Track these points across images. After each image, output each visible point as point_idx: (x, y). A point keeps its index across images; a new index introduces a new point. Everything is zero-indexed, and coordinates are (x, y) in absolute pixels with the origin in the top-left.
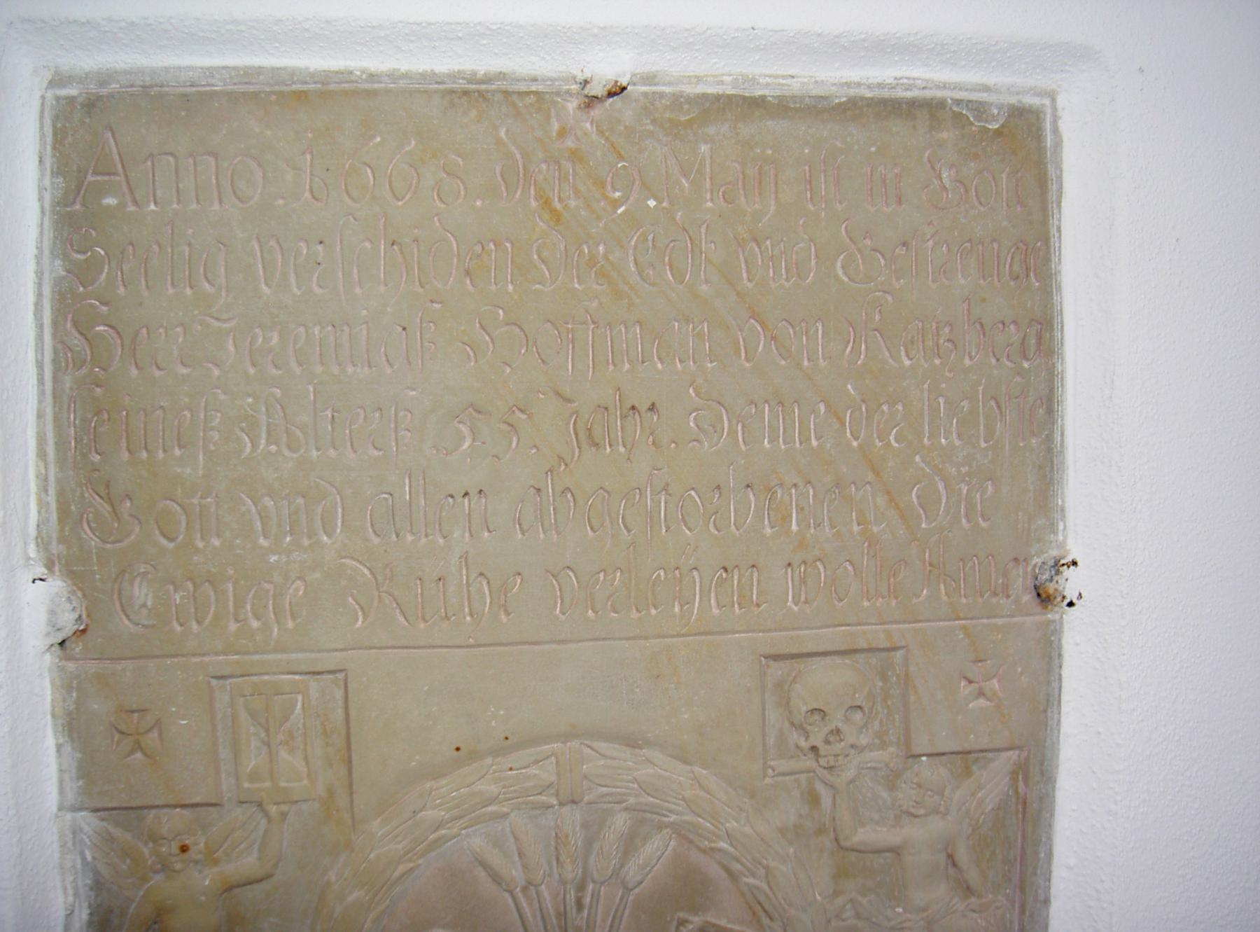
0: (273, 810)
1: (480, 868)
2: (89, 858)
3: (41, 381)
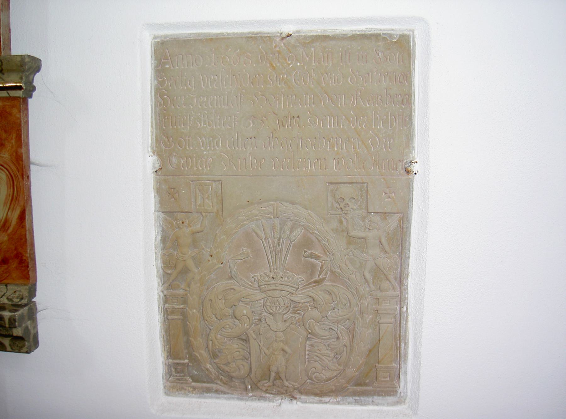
0: (204, 214)
3: (152, 109)
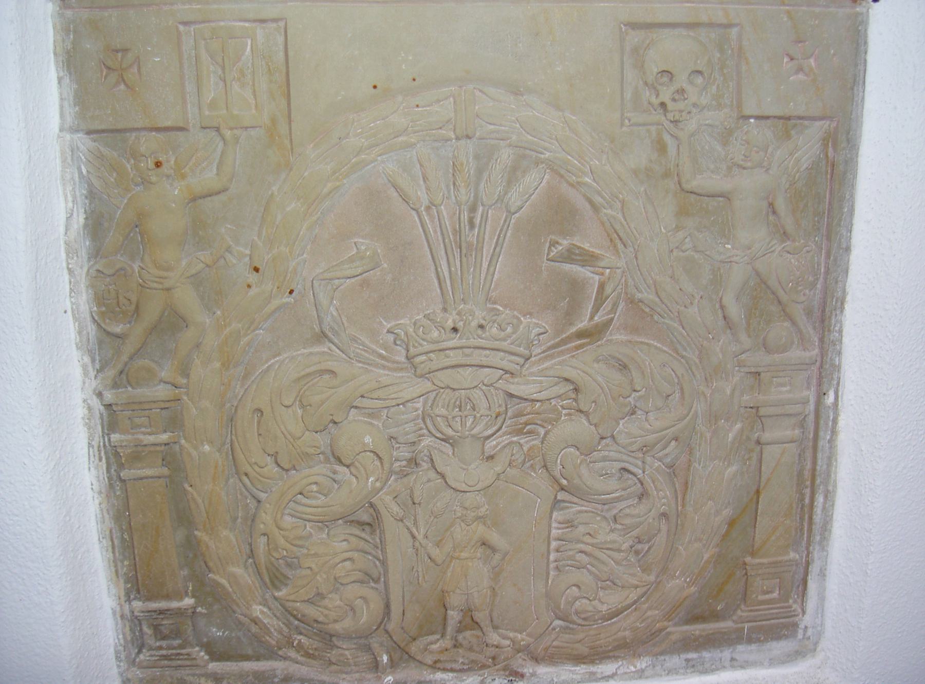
0: (228, 134)
1: (392, 189)
2: (84, 171)
